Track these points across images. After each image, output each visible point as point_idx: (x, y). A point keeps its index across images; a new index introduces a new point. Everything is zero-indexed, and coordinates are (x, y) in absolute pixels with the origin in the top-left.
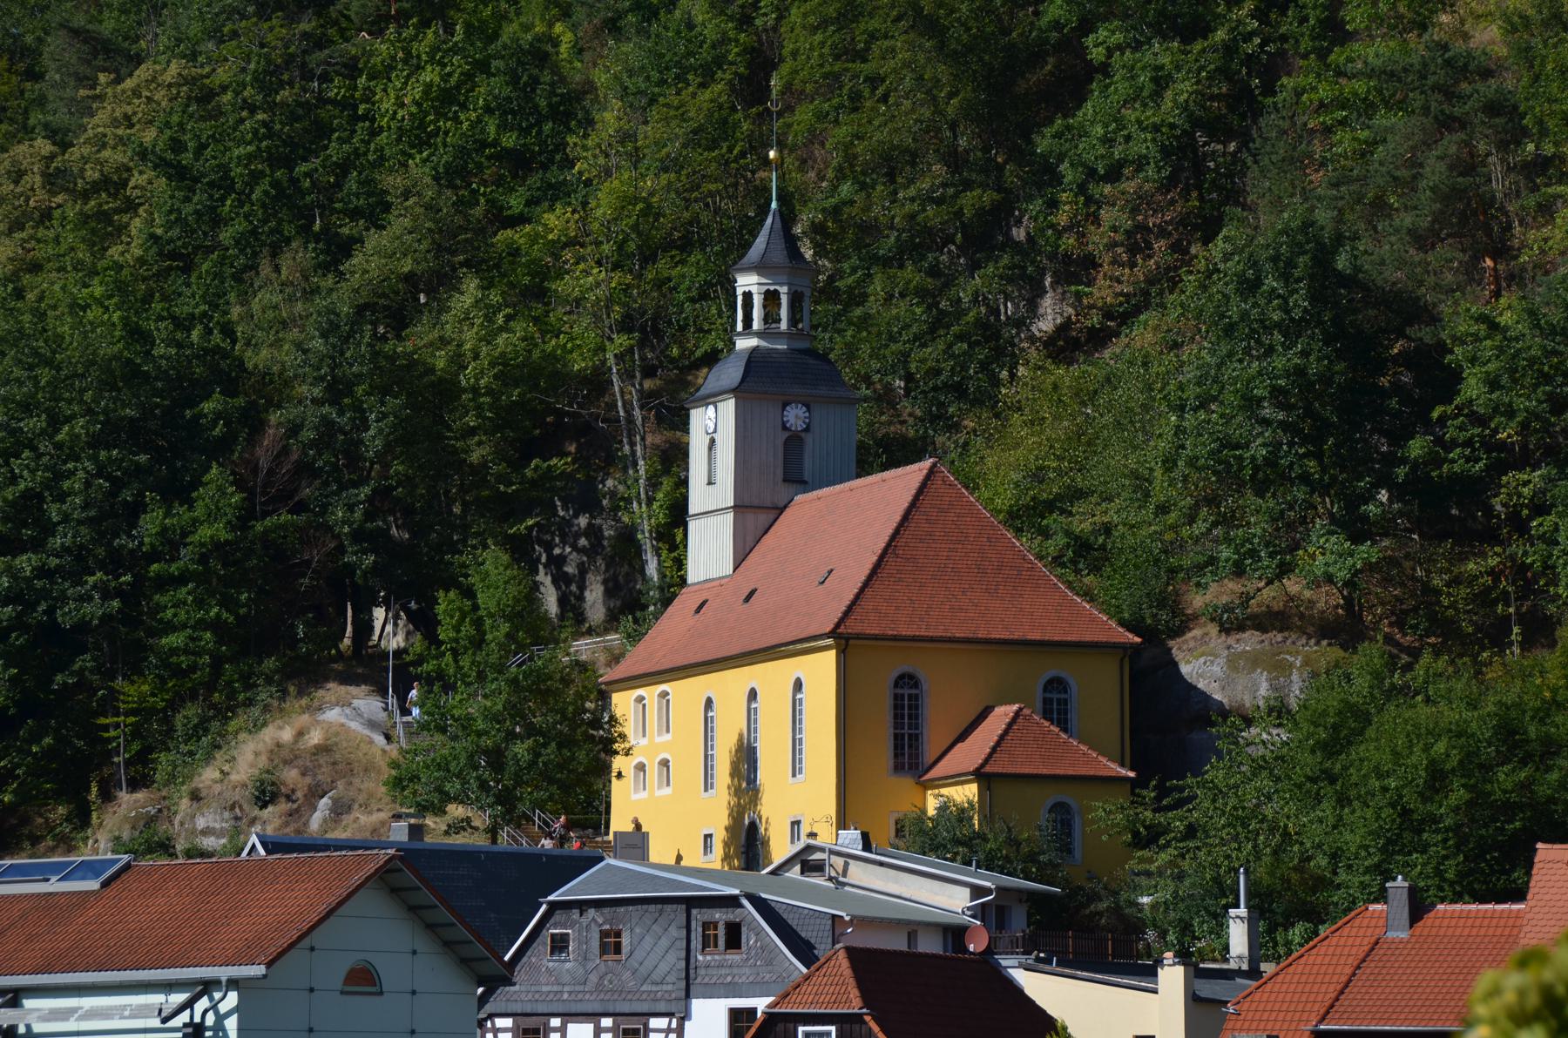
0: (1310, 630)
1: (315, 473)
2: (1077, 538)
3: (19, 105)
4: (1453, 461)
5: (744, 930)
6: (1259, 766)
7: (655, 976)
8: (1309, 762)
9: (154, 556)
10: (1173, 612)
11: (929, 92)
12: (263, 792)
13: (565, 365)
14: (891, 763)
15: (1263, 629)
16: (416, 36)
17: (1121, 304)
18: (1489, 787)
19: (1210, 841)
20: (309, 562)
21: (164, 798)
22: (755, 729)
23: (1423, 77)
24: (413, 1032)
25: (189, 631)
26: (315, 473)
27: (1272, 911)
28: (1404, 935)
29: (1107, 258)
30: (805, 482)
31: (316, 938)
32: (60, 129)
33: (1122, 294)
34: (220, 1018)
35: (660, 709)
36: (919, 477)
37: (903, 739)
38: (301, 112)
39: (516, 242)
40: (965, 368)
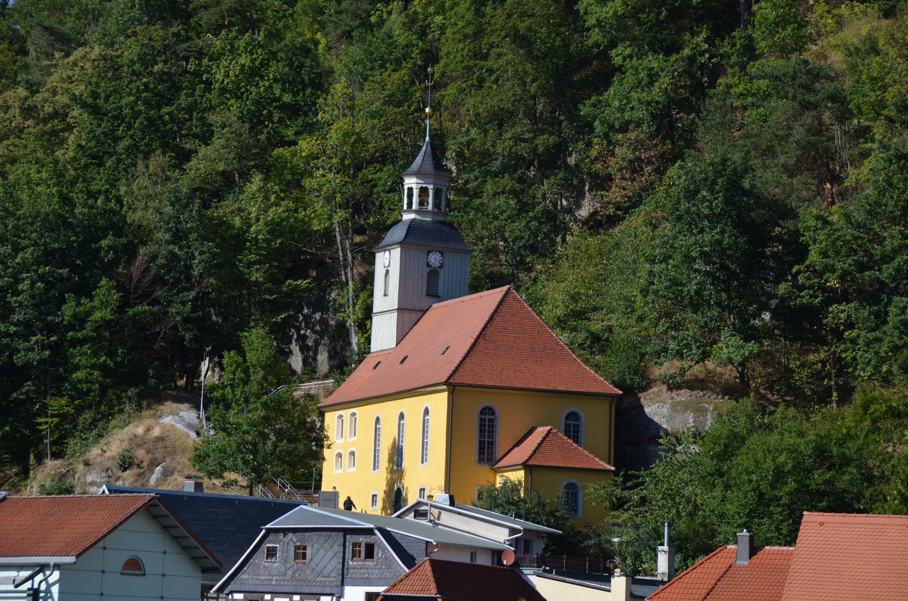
0: (718, 390)
1: (164, 283)
2: (592, 334)
3: (12, 69)
4: (803, 297)
5: (376, 548)
7: (325, 573)
8: (709, 465)
9: (70, 327)
10: (642, 377)
13: (309, 226)
14: (477, 457)
15: (691, 388)
17: (625, 202)
19: (653, 507)
20: (158, 333)
22: (403, 436)
23: (794, 79)
24: (162, 598)
25: (88, 369)
26: (164, 283)
27: (686, 549)
28: (746, 563)
29: (619, 176)
30: (439, 297)
31: (107, 542)
32: (35, 84)
33: (626, 196)
34: (49, 586)
35: (351, 422)
36: (500, 296)
40: (536, 236)
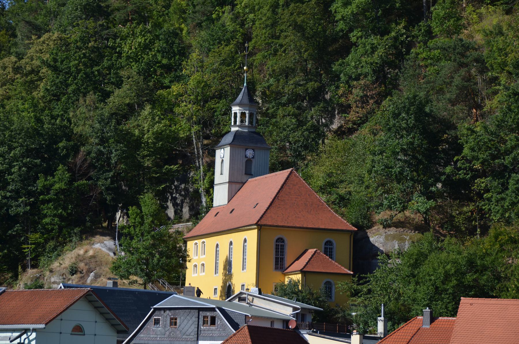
0: (412, 228)
1: (95, 167)
2: (340, 196)
3: (8, 45)
4: (460, 174)
5: (216, 319)
6: (391, 271)
7: (187, 333)
8: (407, 270)
10: (369, 221)
11: (298, 50)
12: (73, 270)
13: (178, 135)
15: (397, 227)
16: (136, 26)
17: (358, 120)
18: (464, 280)
20: (92, 196)
21: (42, 271)
23: (454, 49)
26: (95, 167)
27: (394, 319)
28: (428, 327)
30: (252, 175)
31: (63, 316)
32: (21, 54)
33: (359, 117)
35: (202, 247)
36: (287, 174)
37: (278, 259)
38: (95, 50)
39: (163, 94)
